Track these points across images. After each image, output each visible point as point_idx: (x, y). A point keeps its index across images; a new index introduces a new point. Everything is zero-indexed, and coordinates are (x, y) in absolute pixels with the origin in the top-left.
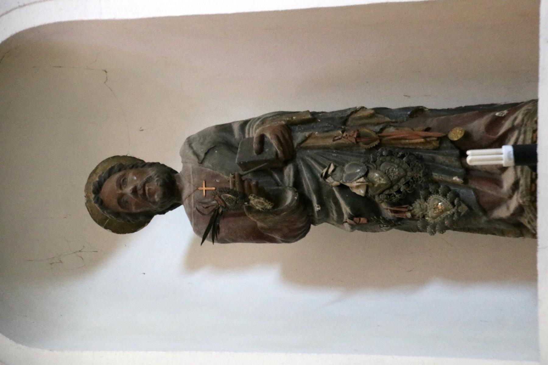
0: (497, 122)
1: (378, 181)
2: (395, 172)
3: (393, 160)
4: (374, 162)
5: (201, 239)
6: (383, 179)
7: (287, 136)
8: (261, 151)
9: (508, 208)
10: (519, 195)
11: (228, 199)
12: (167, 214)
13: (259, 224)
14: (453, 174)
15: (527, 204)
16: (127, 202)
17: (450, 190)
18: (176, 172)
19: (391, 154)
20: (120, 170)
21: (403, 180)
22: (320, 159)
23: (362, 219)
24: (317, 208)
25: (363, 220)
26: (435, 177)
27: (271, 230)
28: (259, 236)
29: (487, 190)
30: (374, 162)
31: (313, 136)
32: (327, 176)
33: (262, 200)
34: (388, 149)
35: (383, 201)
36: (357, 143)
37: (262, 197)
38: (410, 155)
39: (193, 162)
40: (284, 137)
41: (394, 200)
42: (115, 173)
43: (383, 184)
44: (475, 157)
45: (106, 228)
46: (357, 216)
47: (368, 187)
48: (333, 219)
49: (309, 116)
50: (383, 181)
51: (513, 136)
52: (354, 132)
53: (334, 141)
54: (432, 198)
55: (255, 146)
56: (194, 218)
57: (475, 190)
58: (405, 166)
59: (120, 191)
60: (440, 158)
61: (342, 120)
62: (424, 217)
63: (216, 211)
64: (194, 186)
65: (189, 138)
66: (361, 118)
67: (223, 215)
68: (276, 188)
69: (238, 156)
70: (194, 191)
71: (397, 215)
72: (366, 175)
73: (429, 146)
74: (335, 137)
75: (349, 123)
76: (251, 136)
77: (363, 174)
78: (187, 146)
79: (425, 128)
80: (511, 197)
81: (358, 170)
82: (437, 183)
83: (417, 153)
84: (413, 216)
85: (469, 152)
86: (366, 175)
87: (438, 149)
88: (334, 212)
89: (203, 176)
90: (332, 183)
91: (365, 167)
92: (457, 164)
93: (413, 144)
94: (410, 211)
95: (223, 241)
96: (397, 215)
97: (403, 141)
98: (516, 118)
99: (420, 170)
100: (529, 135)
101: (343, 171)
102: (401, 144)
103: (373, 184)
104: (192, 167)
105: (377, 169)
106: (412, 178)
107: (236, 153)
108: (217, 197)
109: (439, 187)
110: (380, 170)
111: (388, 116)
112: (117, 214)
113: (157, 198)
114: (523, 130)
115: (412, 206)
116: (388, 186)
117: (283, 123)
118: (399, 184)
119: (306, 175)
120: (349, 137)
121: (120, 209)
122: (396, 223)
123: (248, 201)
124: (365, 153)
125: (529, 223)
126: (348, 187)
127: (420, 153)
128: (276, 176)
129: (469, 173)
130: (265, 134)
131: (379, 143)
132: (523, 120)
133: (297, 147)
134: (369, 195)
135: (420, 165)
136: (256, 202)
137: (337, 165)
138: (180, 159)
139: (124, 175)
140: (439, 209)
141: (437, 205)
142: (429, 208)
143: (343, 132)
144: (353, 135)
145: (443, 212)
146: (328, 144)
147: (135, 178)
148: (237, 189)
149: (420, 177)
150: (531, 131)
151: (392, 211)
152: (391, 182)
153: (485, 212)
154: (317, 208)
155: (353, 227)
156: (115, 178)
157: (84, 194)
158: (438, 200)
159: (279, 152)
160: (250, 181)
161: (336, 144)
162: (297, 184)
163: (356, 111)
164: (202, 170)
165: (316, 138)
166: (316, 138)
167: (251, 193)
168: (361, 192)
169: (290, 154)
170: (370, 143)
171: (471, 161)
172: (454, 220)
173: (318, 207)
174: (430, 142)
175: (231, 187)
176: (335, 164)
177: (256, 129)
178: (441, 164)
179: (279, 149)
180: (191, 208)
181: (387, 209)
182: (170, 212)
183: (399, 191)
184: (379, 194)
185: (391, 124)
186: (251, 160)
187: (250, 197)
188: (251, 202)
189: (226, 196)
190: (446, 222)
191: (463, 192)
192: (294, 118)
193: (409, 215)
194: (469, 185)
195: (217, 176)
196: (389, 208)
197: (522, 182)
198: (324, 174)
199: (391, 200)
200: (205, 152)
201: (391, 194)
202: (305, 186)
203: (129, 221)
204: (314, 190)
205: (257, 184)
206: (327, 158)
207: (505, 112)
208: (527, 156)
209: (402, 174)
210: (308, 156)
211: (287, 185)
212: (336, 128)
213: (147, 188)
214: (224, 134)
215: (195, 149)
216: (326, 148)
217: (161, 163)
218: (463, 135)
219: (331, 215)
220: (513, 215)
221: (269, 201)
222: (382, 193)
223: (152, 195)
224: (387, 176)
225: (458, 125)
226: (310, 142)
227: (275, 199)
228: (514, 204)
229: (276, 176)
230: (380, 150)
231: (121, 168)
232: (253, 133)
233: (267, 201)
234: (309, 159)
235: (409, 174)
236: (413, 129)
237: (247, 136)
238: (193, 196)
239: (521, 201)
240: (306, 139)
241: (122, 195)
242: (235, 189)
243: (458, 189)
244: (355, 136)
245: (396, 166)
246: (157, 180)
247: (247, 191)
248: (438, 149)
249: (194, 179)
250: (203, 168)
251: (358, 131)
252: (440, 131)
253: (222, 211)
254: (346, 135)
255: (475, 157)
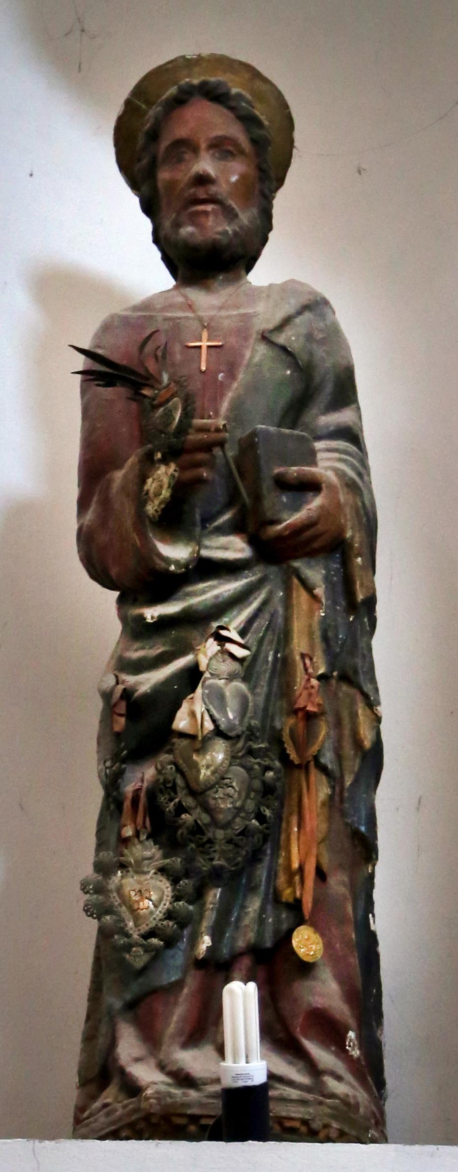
0: (330, 1031)
1: (204, 762)
2: (225, 801)
3: (252, 795)
4: (251, 752)
5: (86, 346)
6: (209, 773)
7: (316, 545)
8: (282, 484)
9: (137, 1060)
10: (163, 1088)
11: (169, 415)
12: (154, 248)
13: (118, 476)
14: (217, 933)
15: (144, 1105)
16: (180, 160)
17: (182, 925)
18: (249, 269)
19: (268, 790)
20: (254, 141)
21: (205, 818)
22: (261, 623)
23: (122, 720)
24: (151, 613)
25: (121, 723)
26: (212, 893)
27: (106, 504)
28: (94, 471)
29: (178, 1014)
30: (251, 752)
31: (316, 606)
32: (222, 640)
33: (166, 493)
34: (278, 784)
35: (159, 772)
36: (296, 712)
37: (172, 496)
38: (262, 840)
39: (266, 315)
40: (315, 538)
41: (162, 799)
42: (248, 131)
43: (199, 771)
44: (241, 1000)
45: (128, 103)
46: (128, 707)
47: (193, 737)
48: (128, 650)
49: (360, 597)
50: (204, 773)
51: (299, 1071)
52: (319, 705)
53: (303, 656)
54: (165, 886)
55: (294, 470)
56: (139, 318)
57: (179, 985)
58: (239, 825)
59: (203, 146)
60: (254, 905)
61: (351, 673)
62: (123, 866)
63: (149, 380)
64: (212, 318)
65: (326, 302)
66: (354, 716)
67: (137, 396)
68: (198, 517)
69: (272, 429)
70: (200, 319)
71: (127, 804)
72: (218, 732)
73: (282, 879)
74: (311, 659)
75: (345, 688)
76: (319, 456)
77: (223, 727)
78: (304, 300)
79: (325, 867)
80: (162, 1067)
81: (231, 716)
82: (198, 896)
83: (269, 852)
84: (125, 841)
85: (252, 986)
86: (218, 732)
87: (275, 898)
88: (140, 654)
89: (232, 341)
90: (205, 654)
91: (239, 730)
92: (241, 944)
93: (288, 839)
94: (137, 834)
95: (83, 392)
96: (127, 804)
97: (294, 820)
98: (339, 1078)
99: (228, 860)
100: (297, 1112)
101: (231, 677)
102: (291, 814)
103: (197, 751)
104: (256, 315)
105: (233, 758)
106: (210, 841)
107: (279, 426)
108: (174, 387)
109: (190, 902)
110: (230, 765)
111: (356, 782)
112: (154, 136)
113: (187, 230)
114: (310, 1097)
115: (148, 838)
116: (193, 785)
117: (349, 534)
118: (198, 810)
119: (227, 588)
120: (307, 690)
121: (164, 144)
122: (113, 803)
123: (165, 461)
124: (273, 728)
125: (105, 1106)
126: (193, 690)
127: (268, 858)
128: (226, 517)
129: (217, 970)
130: (323, 494)
131: (292, 762)
132: (333, 1096)
133: (290, 567)
134: (175, 740)
135: (240, 859)
136: (162, 479)
137: (246, 664)
138: (279, 280)
139: (242, 152)
140: (138, 902)
141: (150, 895)
142: (143, 878)
143: (320, 678)
144: (313, 703)
145: (133, 911)
146: (295, 641)
147: (234, 179)
148: (193, 437)
149: (212, 859)
150: (307, 1117)
151: (137, 793)
152: (203, 792)
153: (131, 1006)
154: (151, 613)
155: (107, 696)
156: (235, 131)
157: (205, 52)
158: (161, 900)
159: (279, 527)
160: (210, 464)
161: (294, 661)
162: (207, 569)
163: (371, 704)
164: (246, 339)
165: (311, 613)
166: (311, 613)
167: (182, 468)
168: (181, 722)
169: (276, 552)
170: (294, 742)
171: (231, 992)
172: (112, 936)
173: (152, 618)
174: (290, 883)
175: (197, 422)
176: (249, 659)
177: (336, 471)
178: (243, 907)
179: (286, 528)
180: (163, 309)
181: (142, 781)
182: (158, 255)
183: (181, 809)
184: (175, 764)
185: (337, 789)
186: (262, 462)
187: (173, 466)
188: (162, 469)
189: (176, 409)
190: (108, 918)
191: (177, 958)
192: (359, 560)
193: (128, 832)
194: (192, 972)
195: (232, 375)
196: (145, 785)
197: (193, 1094)
198: (224, 633)
199: (161, 791)
200: (287, 345)
201: (176, 793)
202: (201, 586)
203: (139, 160)
204: (190, 607)
205: (200, 481)
206: (263, 638)
207: (356, 1053)
208: (244, 1115)
209: (221, 817)
210: (271, 594)
211: (207, 542)
212: (332, 659)
213: (209, 208)
214: (329, 388)
215: (298, 320)
216: (285, 637)
217: (271, 235)
218: (306, 959)
219: (137, 645)
220: (122, 1072)
221: (163, 510)
222: (179, 770)
223: (194, 218)
224: (217, 783)
225: (328, 946)
226: (301, 598)
227: (175, 520)
228: (147, 1075)
229: (226, 517)
230: (277, 764)
231: (259, 144)
232: (328, 462)
233: (163, 506)
234: (262, 596)
235: (220, 834)
236: (323, 840)
237: (319, 445)
238: (190, 315)
239: (149, 1092)
240: (309, 589)
241: (195, 150)
242: (191, 431)
243: (183, 944)
244: (310, 708)
245: (238, 804)
246: (226, 232)
247: (186, 458)
248: (275, 898)
249: (228, 317)
250: (252, 341)
251: (323, 713)
252: (316, 902)
253: (145, 396)
254: (312, 687)
255: (241, 1000)
